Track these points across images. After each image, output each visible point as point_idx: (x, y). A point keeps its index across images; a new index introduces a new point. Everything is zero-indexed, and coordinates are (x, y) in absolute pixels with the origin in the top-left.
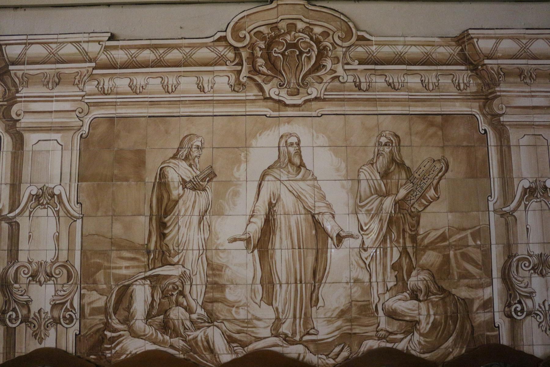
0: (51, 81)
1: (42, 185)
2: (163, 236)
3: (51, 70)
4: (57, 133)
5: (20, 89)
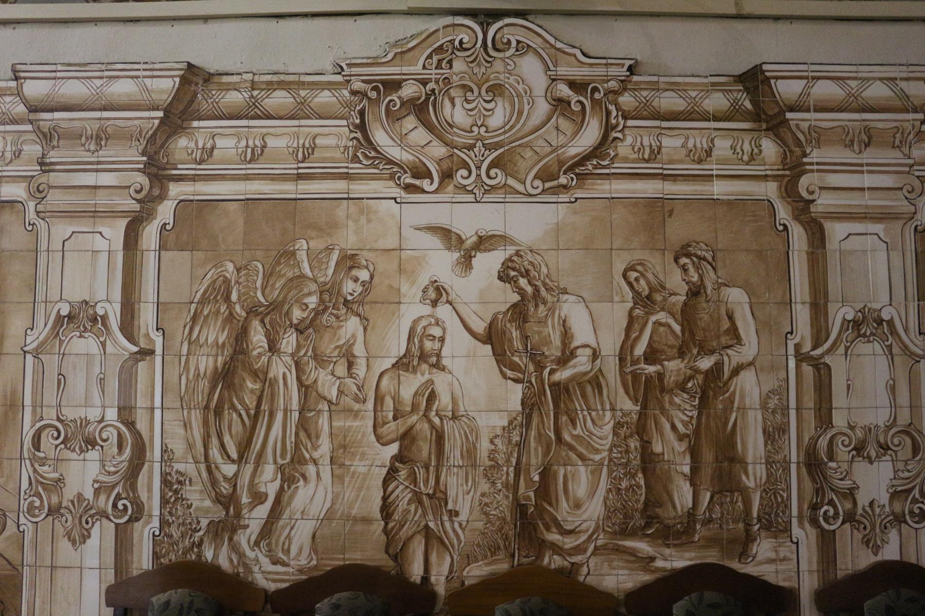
0: (856, 139)
1: (862, 305)
3: (855, 123)
4: (878, 223)
5: (808, 151)
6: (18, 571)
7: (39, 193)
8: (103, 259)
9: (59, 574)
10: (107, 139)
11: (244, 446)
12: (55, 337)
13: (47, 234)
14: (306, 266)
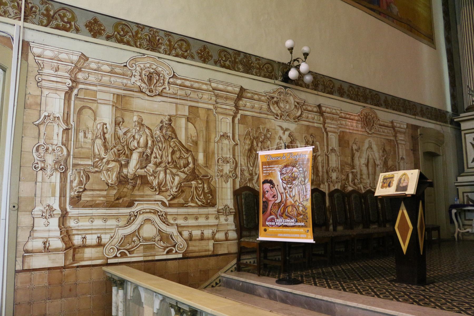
2: (353, 162)
7: (216, 108)
8: (228, 124)
9: (223, 189)
11: (254, 164)
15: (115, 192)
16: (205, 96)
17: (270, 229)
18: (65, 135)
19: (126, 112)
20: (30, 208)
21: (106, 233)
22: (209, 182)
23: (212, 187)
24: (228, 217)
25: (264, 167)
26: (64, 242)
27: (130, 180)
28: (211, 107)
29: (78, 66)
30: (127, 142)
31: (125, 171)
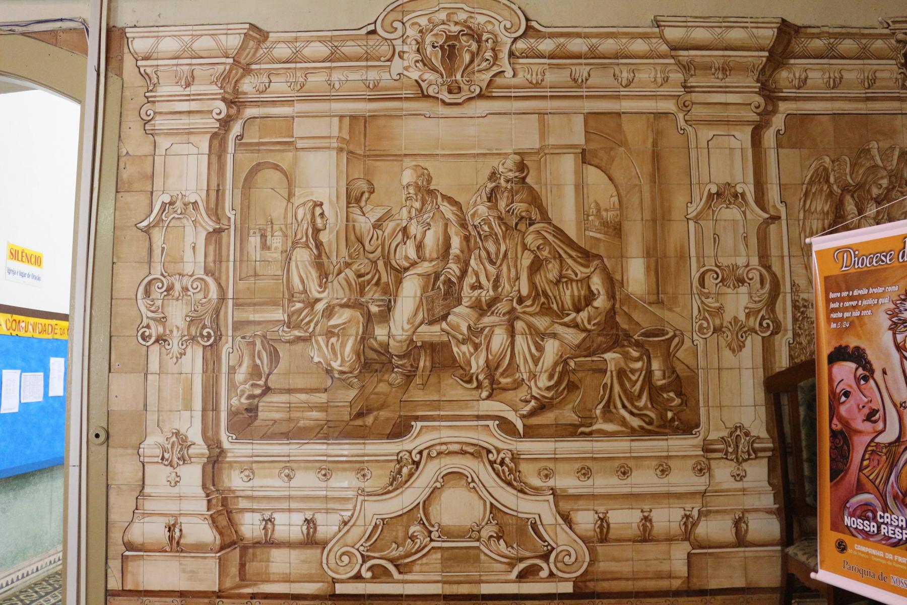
6: (694, 372)
7: (685, 107)
8: (738, 154)
9: (724, 374)
10: (730, 70)
12: (709, 208)
13: (695, 136)
14: (878, 158)
15: (352, 394)
16: (643, 76)
17: (859, 548)
18: (211, 248)
19: (378, 164)
20: (134, 440)
21: (327, 511)
22: (669, 354)
23: (679, 368)
24: (745, 465)
25: (832, 295)
26: (217, 528)
27: (395, 360)
28: (669, 106)
29: (243, 61)
30: (383, 249)
31: (380, 332)
